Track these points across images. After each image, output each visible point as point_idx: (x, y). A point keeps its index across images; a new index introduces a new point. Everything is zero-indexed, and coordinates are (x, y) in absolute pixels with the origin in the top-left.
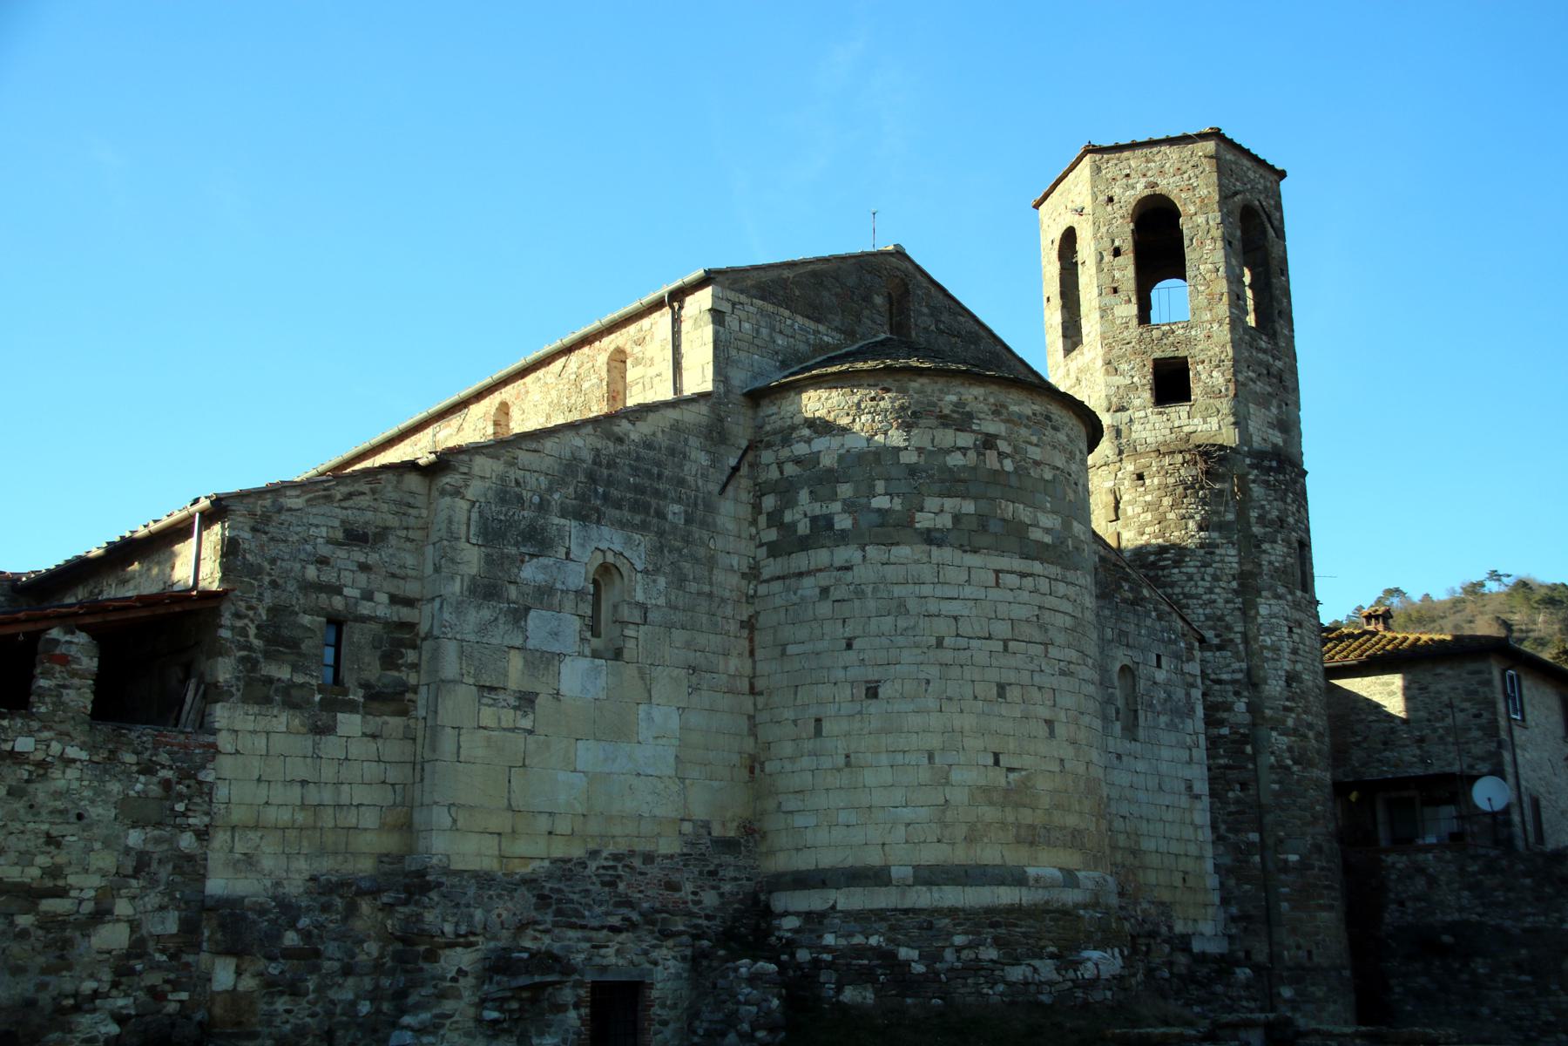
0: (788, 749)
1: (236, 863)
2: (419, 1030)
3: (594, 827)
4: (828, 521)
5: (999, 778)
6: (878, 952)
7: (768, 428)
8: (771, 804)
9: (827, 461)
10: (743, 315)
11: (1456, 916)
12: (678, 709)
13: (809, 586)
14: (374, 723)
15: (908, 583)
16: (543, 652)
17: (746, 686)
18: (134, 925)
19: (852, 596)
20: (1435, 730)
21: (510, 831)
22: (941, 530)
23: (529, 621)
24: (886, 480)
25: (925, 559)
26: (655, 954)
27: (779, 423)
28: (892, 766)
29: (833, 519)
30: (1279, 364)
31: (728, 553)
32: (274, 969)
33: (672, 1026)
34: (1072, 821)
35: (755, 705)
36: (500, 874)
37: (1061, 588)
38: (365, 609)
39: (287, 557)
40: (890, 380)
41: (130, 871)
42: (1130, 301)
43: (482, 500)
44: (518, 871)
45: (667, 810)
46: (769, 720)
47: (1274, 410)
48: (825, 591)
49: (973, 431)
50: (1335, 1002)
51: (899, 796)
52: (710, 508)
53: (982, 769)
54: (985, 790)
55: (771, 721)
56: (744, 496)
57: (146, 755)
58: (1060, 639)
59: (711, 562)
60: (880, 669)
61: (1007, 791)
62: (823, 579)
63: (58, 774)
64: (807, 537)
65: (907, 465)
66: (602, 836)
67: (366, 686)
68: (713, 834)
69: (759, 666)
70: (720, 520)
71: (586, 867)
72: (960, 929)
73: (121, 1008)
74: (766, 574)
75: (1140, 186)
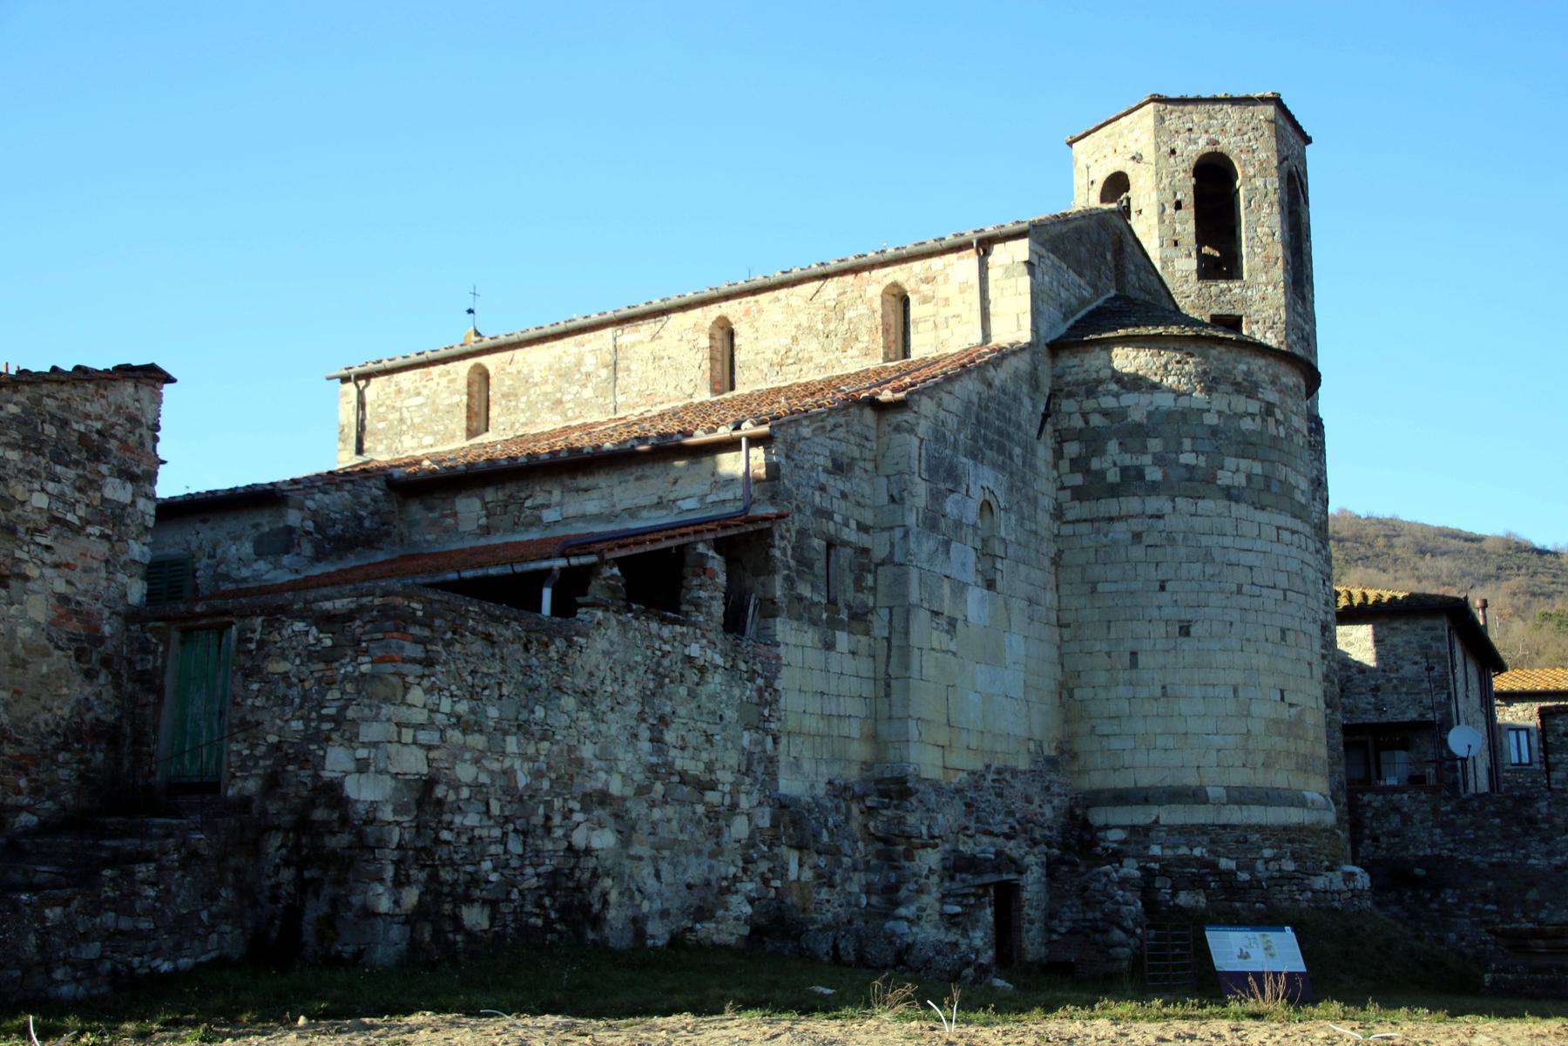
0: (1102, 677)
4: (1139, 473)
5: (1286, 713)
6: (1201, 862)
7: (1069, 378)
9: (1137, 416)
11: (1428, 851)
13: (1120, 531)
19: (1165, 543)
20: (1389, 680)
25: (1227, 514)
27: (1081, 377)
33: (1037, 925)
40: (1193, 346)
42: (1190, 255)
45: (1021, 731)
48: (1137, 537)
49: (1259, 399)
54: (1277, 722)
55: (1081, 651)
62: (1136, 525)
64: (1118, 485)
65: (1210, 426)
72: (1267, 843)
74: (1070, 515)
75: (1202, 142)
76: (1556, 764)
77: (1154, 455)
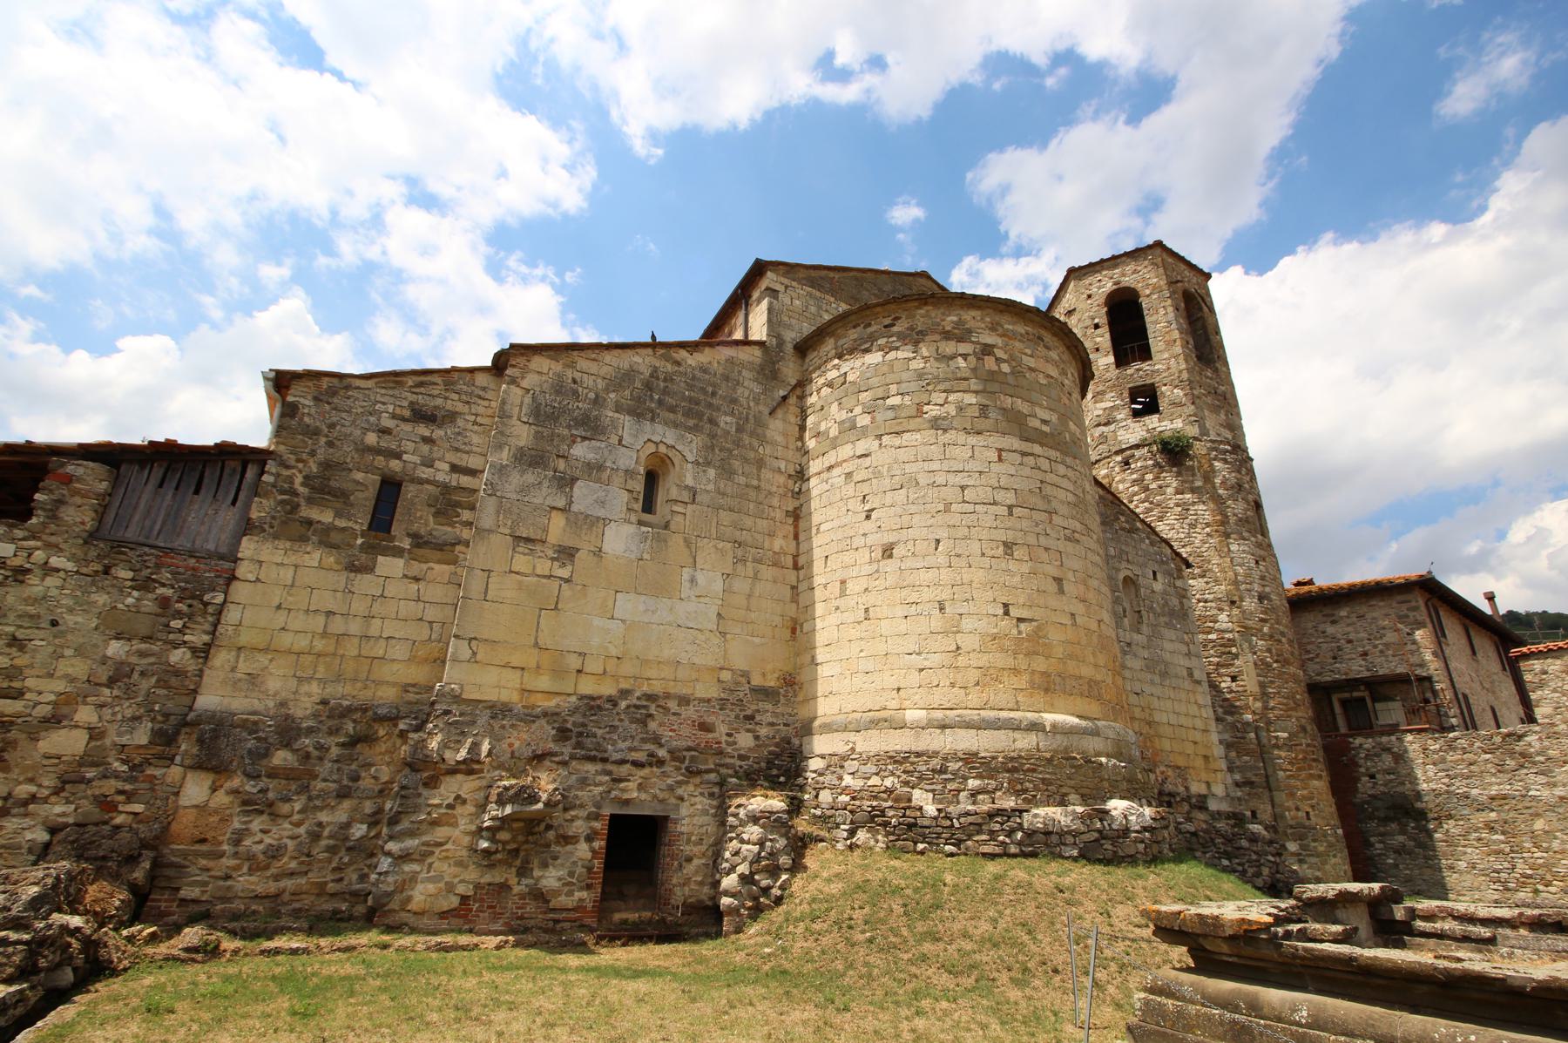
1: (236, 683)
2: (401, 857)
3: (628, 668)
10: (794, 295)
14: (417, 568)
16: (587, 516)
18: (95, 734)
20: (1375, 647)
23: (575, 489)
26: (680, 791)
30: (1223, 388)
32: (251, 787)
34: (1087, 671)
37: (1062, 470)
38: (424, 473)
39: (347, 424)
41: (104, 679)
43: (538, 389)
47: (1223, 417)
50: (1335, 856)
52: (759, 423)
56: (792, 419)
57: (146, 572)
58: (1063, 510)
62: (847, 467)
63: (35, 580)
64: (836, 438)
66: (636, 678)
67: (415, 536)
70: (769, 433)
73: (58, 815)
76: (1538, 701)
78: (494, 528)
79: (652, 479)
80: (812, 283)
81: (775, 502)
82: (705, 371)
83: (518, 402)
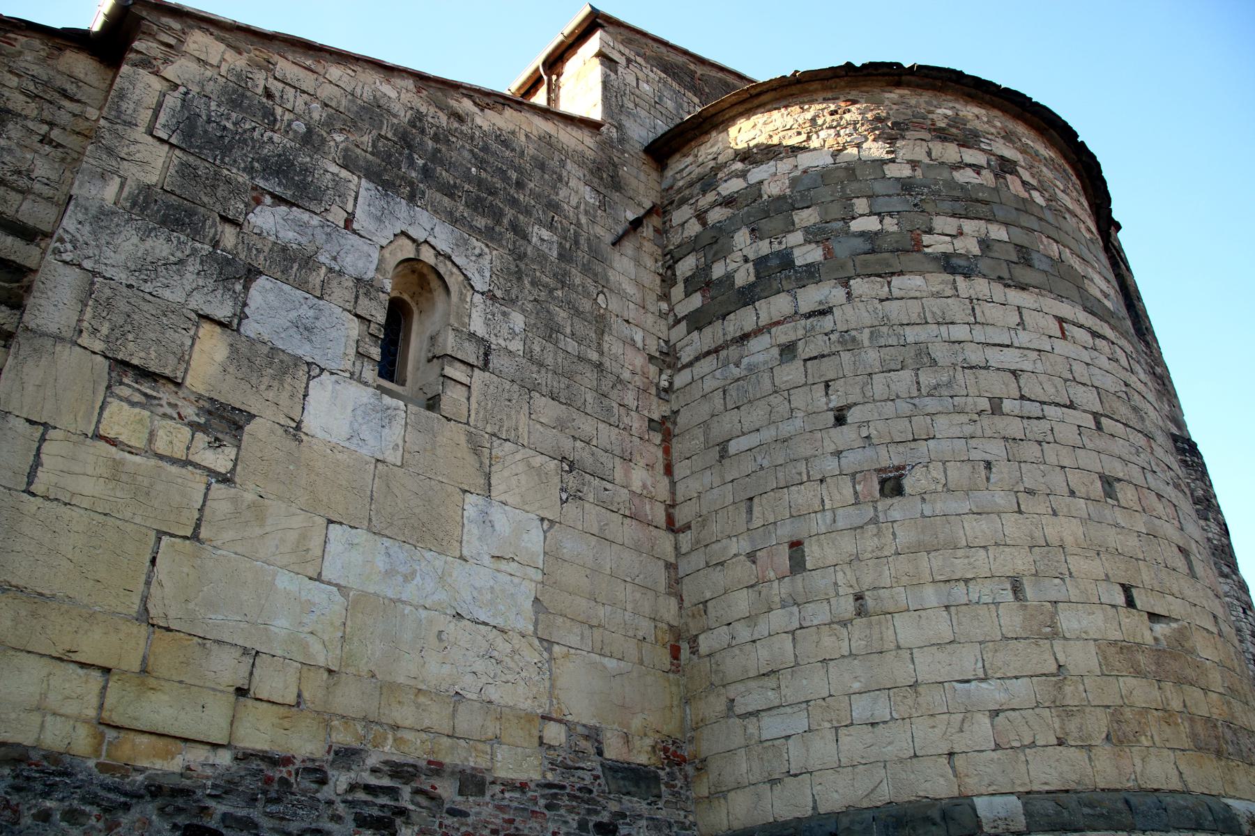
0: (742, 602)
3: (350, 699)
4: (786, 260)
8: (717, 705)
9: (773, 189)
12: (542, 520)
13: (761, 350)
15: (927, 323)
17: (661, 518)
21: (136, 667)
22: (965, 256)
24: (868, 197)
25: (949, 292)
28: (947, 607)
29: (792, 253)
31: (627, 321)
35: (677, 548)
36: (91, 763)
43: (195, 89)
44: (139, 764)
46: (702, 564)
48: (788, 351)
51: (968, 661)
53: (1111, 611)
54: (1126, 648)
55: (708, 565)
59: (601, 323)
60: (901, 448)
61: (1159, 653)
62: (783, 335)
64: (751, 286)
65: (898, 179)
66: (368, 722)
68: (607, 755)
69: (681, 489)
71: (323, 782)
77: (807, 230)
78: (68, 334)
79: (398, 315)
80: (667, 68)
81: (630, 399)
82: (505, 144)
83: (152, 101)
